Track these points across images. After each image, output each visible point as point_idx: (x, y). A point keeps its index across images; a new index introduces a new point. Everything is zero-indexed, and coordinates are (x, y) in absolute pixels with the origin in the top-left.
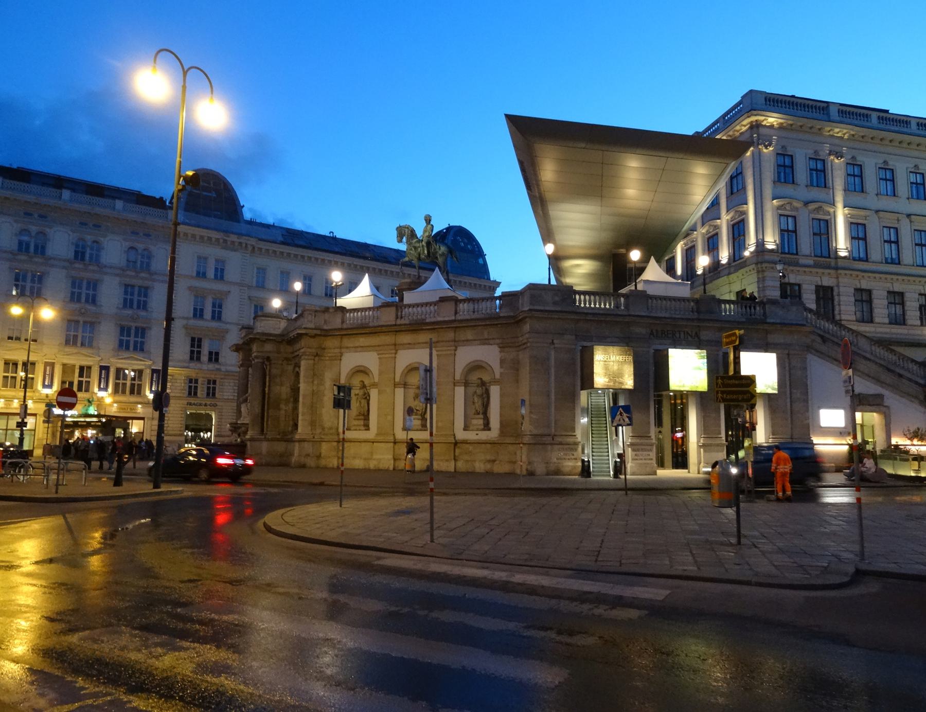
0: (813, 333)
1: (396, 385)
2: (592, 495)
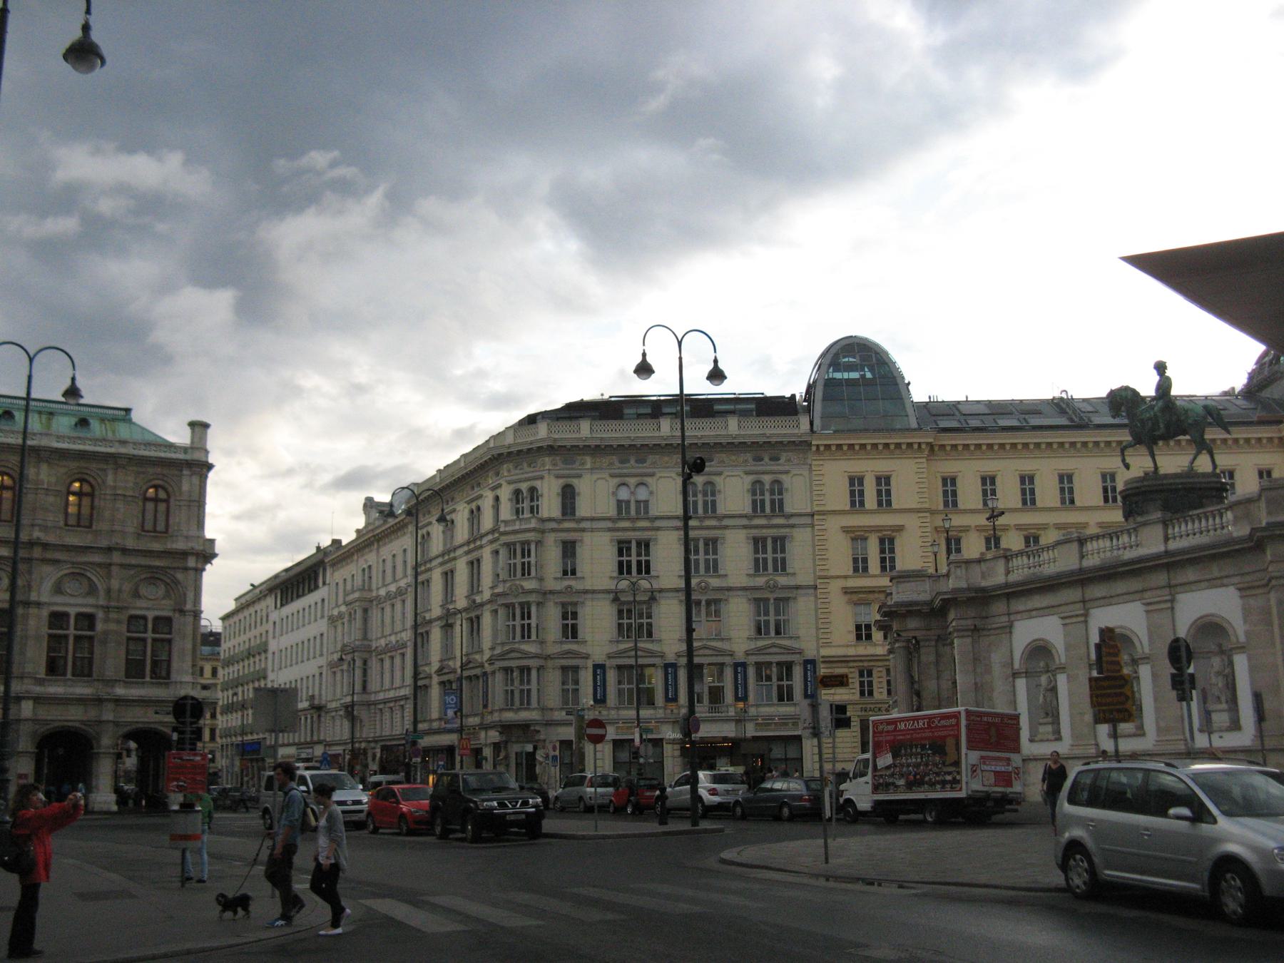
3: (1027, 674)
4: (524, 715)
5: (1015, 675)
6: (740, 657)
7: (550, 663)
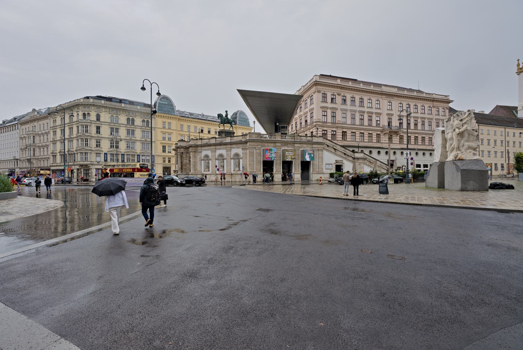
2: (150, 145)
3: (234, 159)
4: (86, 163)
6: (138, 154)
7: (93, 152)
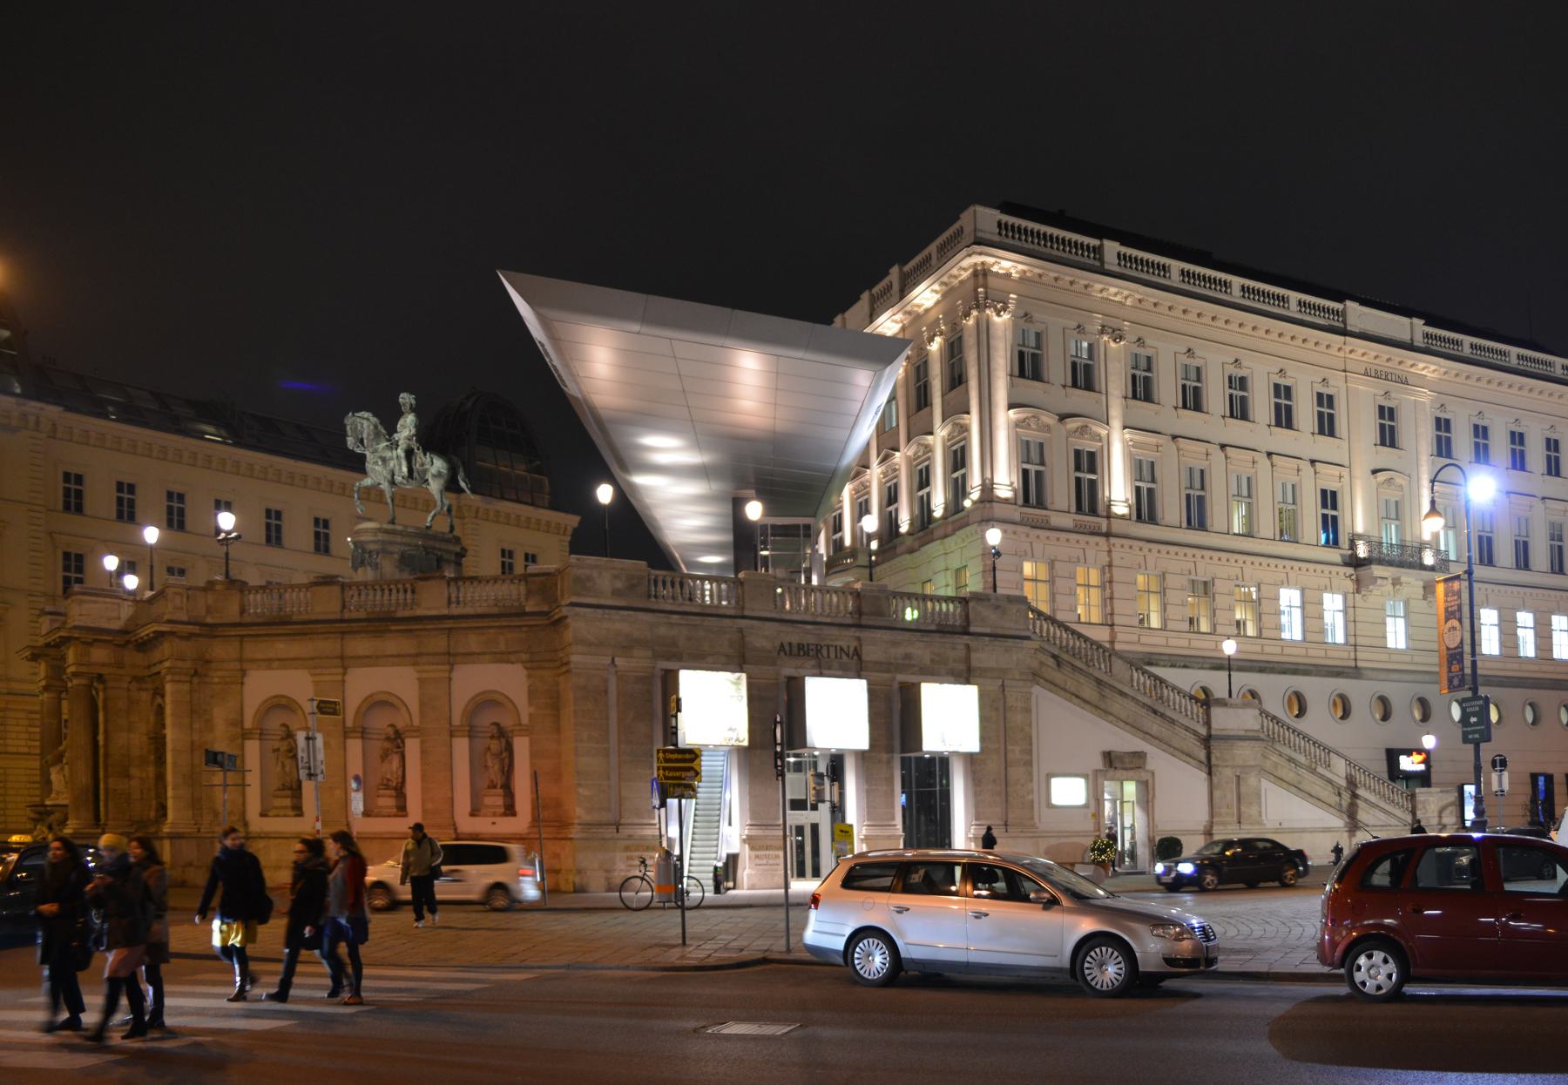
0: (1042, 650)
1: (346, 734)
5: (246, 735)
